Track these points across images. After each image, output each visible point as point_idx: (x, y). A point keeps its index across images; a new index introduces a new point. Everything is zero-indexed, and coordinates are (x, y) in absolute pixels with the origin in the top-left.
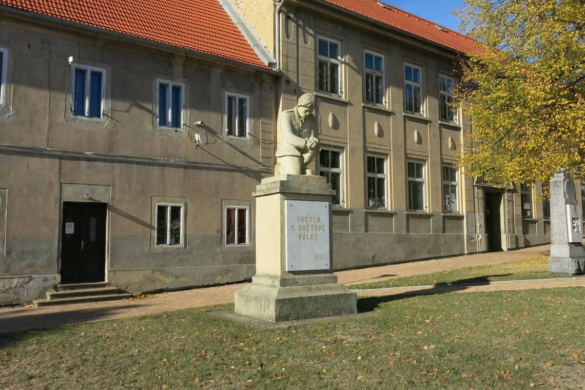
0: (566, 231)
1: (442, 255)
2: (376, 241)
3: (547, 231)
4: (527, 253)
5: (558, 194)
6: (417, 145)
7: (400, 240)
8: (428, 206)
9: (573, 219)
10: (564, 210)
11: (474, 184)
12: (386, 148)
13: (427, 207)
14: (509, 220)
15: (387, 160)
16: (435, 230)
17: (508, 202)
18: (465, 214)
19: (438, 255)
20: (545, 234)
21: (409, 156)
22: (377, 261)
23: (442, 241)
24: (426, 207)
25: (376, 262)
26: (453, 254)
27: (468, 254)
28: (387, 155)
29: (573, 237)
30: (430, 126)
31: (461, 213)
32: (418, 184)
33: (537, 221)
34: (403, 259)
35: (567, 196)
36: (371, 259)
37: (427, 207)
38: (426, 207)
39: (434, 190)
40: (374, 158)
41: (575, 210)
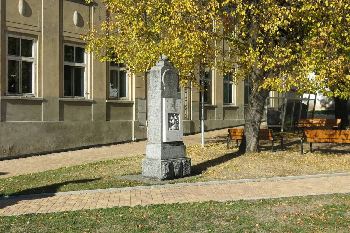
0: (160, 128)
1: (104, 142)
2: (16, 131)
3: (225, 116)
4: (193, 139)
5: (156, 86)
6: (77, 28)
7: (50, 128)
8: (89, 92)
9: (170, 115)
10: (160, 105)
11: (146, 71)
12: (35, 29)
13: (88, 94)
14: (185, 106)
15: (36, 42)
16: (97, 117)
17: (185, 89)
18: (134, 100)
19: (99, 143)
20: (223, 119)
21: (65, 38)
22: (16, 152)
23: (105, 129)
24: (87, 94)
25: (15, 153)
26: (118, 141)
27: (135, 141)
28: (36, 36)
29: (167, 135)
30: (95, 9)
31: (130, 100)
32: (80, 69)
33: (216, 107)
34: (53, 147)
35: (165, 88)
36: (9, 151)
37: (88, 94)
38: (87, 94)
39: (97, 76)
40: (19, 39)
41: (174, 104)
